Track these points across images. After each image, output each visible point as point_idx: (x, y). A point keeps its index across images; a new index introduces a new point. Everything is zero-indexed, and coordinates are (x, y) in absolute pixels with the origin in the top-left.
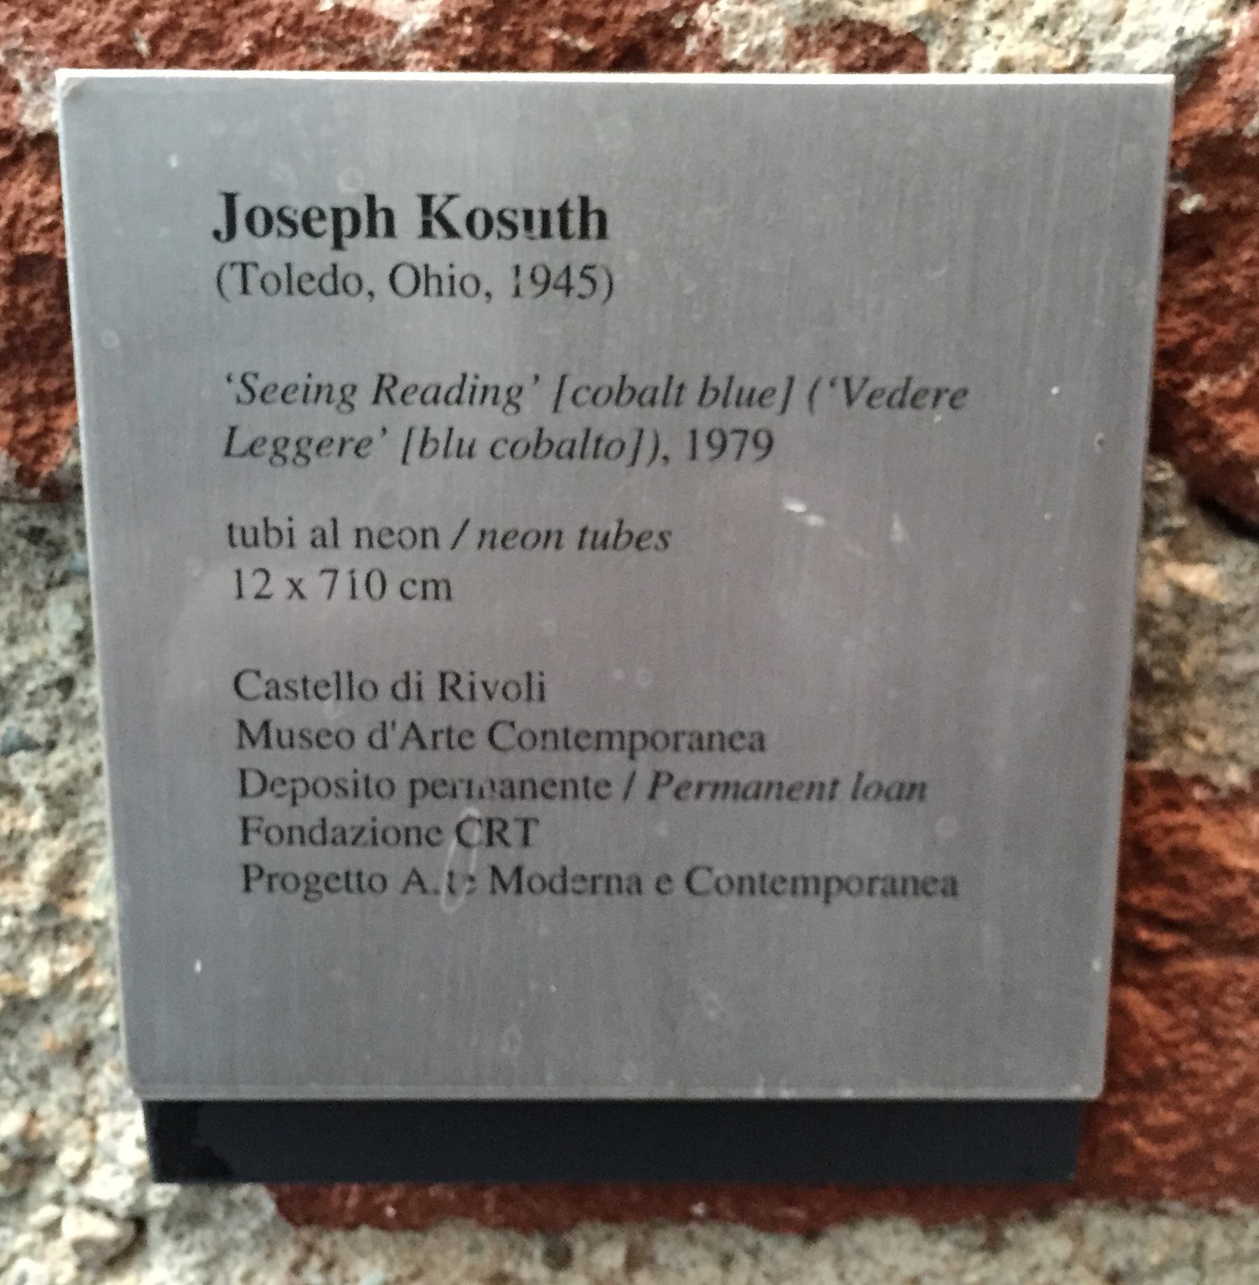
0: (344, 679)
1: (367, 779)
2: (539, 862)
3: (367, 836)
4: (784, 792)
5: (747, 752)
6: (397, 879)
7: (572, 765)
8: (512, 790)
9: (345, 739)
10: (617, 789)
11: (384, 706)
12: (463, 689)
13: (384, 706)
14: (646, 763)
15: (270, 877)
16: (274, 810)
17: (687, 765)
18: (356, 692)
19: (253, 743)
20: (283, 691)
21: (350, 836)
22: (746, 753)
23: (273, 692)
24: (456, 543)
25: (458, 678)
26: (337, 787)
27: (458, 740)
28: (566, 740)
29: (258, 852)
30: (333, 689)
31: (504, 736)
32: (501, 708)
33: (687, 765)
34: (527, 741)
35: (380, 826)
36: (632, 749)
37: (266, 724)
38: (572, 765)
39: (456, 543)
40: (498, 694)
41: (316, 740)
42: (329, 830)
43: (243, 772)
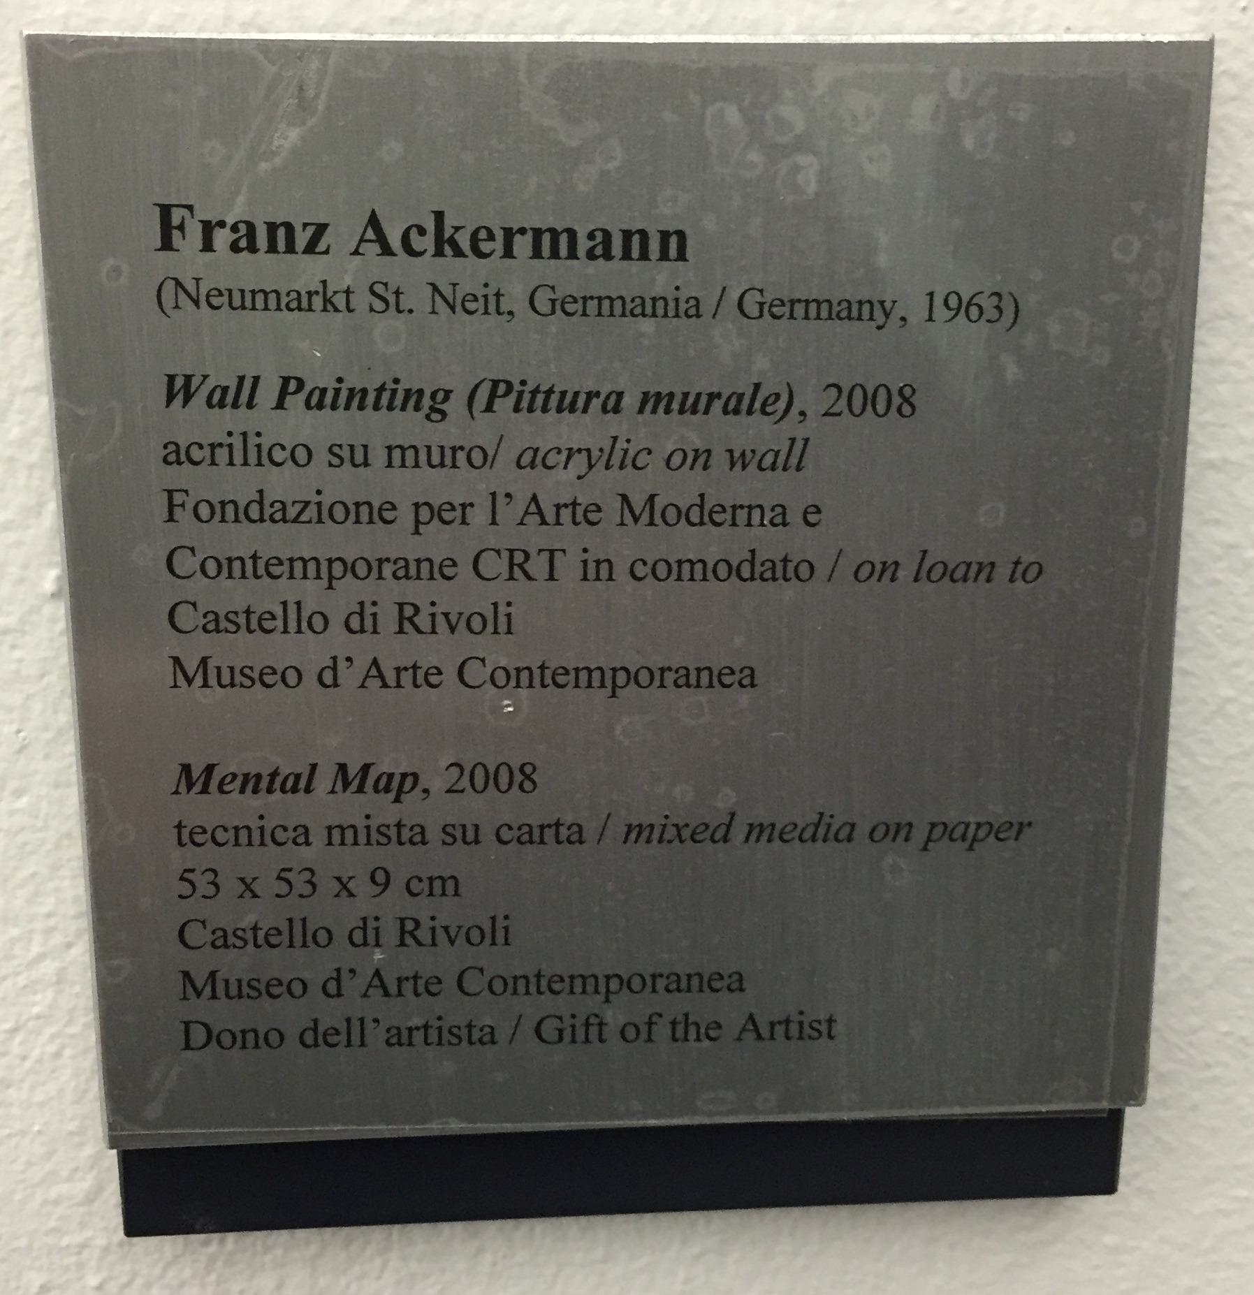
0: (292, 610)
3: (311, 512)
4: (776, 834)
5: (725, 993)
9: (292, 678)
11: (338, 641)
12: (423, 621)
13: (341, 955)
18: (304, 625)
19: (190, 681)
20: (224, 624)
21: (292, 512)
22: (724, 994)
25: (417, 610)
32: (468, 644)
35: (327, 500)
36: (331, 577)
37: (204, 661)
40: (461, 940)
42: (267, 503)
43: (187, 1024)
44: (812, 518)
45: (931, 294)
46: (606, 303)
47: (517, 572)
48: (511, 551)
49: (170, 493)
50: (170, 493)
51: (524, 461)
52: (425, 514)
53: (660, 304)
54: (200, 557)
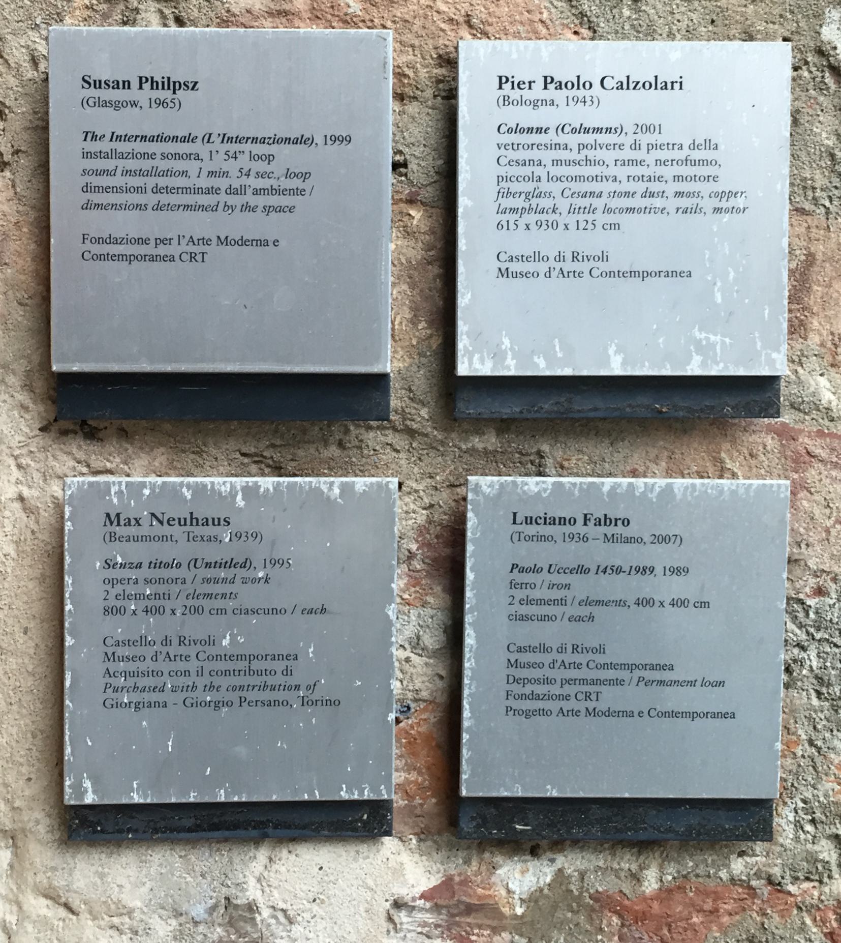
1: (547, 678)
2: (602, 706)
6: (556, 711)
7: (611, 674)
8: (594, 682)
10: (627, 682)
14: (637, 673)
15: (514, 710)
16: (517, 689)
17: (648, 675)
23: (520, 650)
24: (725, 716)
26: (537, 681)
27: (578, 666)
28: (613, 666)
29: (511, 703)
30: (538, 650)
31: (592, 665)
32: (590, 656)
33: (648, 675)
34: (660, 714)
36: (130, 261)
38: (611, 674)
39: (725, 716)
41: (530, 665)
44: (276, 244)
45: (326, 136)
46: (184, 190)
47: (193, 260)
48: (191, 253)
49: (84, 235)
50: (84, 235)
51: (155, 208)
52: (158, 241)
53: (200, 190)
54: (92, 254)
